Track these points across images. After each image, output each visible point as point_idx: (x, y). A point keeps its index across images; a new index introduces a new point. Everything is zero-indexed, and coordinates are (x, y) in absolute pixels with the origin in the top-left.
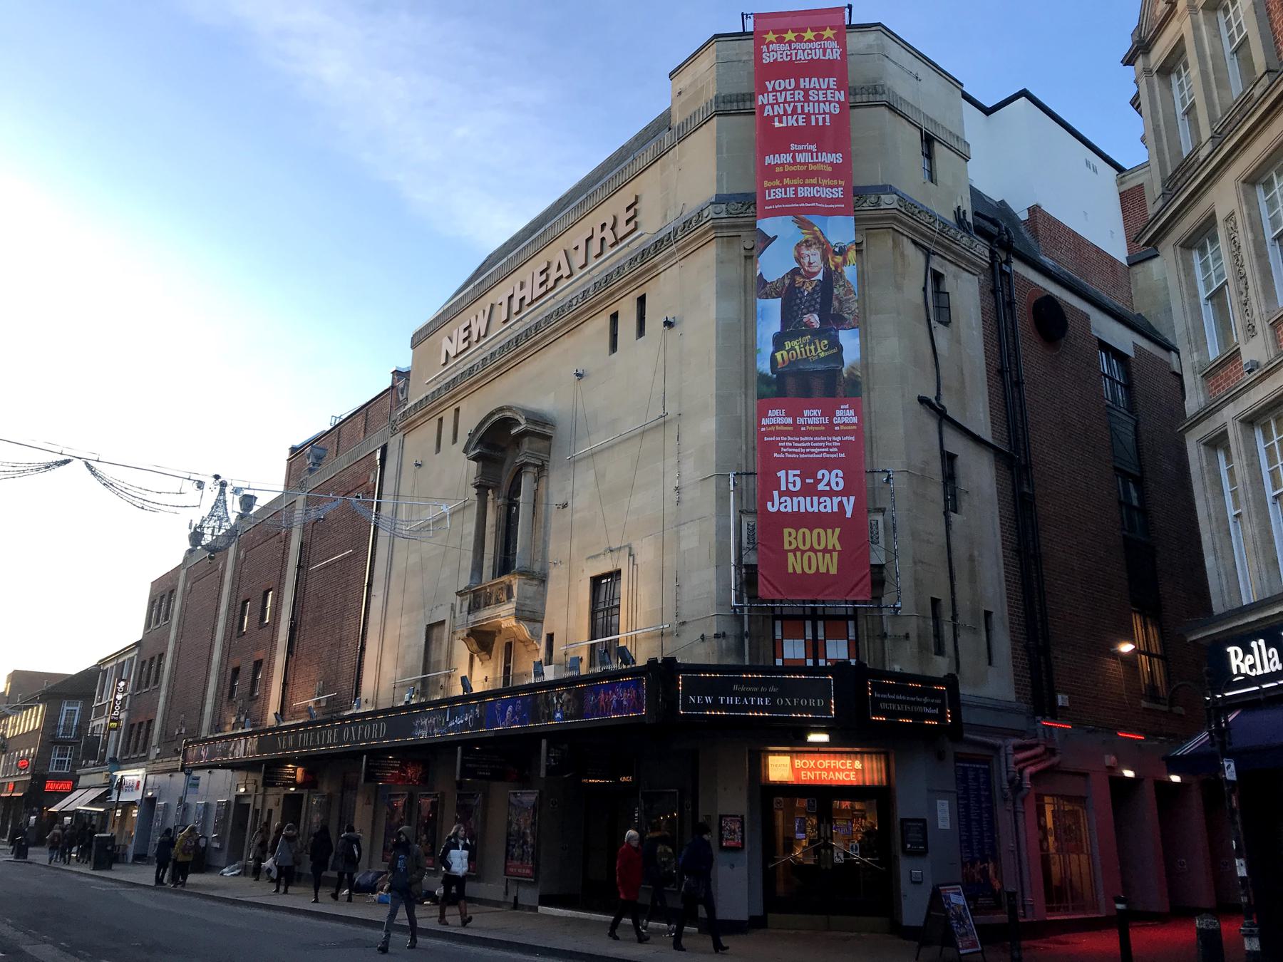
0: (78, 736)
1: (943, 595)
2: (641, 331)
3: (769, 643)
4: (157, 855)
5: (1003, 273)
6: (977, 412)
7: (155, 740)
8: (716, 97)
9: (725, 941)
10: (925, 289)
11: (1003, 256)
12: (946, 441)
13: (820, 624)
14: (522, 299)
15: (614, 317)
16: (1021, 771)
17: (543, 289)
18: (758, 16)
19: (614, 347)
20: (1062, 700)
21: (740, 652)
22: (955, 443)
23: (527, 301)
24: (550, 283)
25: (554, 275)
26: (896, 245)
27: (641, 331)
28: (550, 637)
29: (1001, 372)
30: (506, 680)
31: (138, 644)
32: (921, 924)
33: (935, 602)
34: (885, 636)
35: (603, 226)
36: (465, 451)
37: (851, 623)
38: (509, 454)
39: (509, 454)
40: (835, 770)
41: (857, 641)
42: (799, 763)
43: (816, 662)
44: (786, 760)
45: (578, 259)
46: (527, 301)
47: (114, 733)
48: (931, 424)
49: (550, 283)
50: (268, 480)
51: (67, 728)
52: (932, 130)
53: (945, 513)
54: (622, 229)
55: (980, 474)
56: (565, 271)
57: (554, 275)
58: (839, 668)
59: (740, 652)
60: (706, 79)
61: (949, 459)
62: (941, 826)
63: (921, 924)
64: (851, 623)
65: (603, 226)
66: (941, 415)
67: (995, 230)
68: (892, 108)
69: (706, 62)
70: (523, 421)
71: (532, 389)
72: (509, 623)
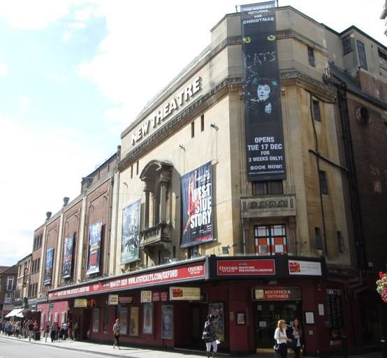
0: (13, 290)
1: (319, 225)
2: (203, 129)
3: (253, 247)
5: (343, 99)
6: (334, 154)
7: (39, 291)
10: (311, 108)
11: (343, 92)
12: (320, 166)
14: (160, 118)
17: (167, 114)
19: (193, 135)
22: (324, 166)
23: (162, 119)
24: (170, 112)
25: (171, 108)
26: (298, 92)
27: (203, 129)
29: (344, 138)
30: (184, 177)
31: (31, 255)
32: (312, 313)
33: (317, 229)
34: (297, 243)
35: (188, 89)
36: (140, 178)
40: (281, 294)
41: (286, 245)
43: (271, 254)
44: (262, 291)
45: (179, 102)
48: (314, 157)
50: (74, 191)
51: (10, 286)
52: (311, 45)
53: (321, 195)
54: (195, 90)
55: (336, 180)
56: (175, 107)
57: (171, 108)
58: (278, 255)
60: (223, 32)
61: (322, 174)
63: (312, 313)
64: (284, 238)
65: (188, 89)
66: (318, 156)
67: (339, 83)
68: (294, 38)
69: (224, 27)
70: (160, 166)
71: (160, 154)
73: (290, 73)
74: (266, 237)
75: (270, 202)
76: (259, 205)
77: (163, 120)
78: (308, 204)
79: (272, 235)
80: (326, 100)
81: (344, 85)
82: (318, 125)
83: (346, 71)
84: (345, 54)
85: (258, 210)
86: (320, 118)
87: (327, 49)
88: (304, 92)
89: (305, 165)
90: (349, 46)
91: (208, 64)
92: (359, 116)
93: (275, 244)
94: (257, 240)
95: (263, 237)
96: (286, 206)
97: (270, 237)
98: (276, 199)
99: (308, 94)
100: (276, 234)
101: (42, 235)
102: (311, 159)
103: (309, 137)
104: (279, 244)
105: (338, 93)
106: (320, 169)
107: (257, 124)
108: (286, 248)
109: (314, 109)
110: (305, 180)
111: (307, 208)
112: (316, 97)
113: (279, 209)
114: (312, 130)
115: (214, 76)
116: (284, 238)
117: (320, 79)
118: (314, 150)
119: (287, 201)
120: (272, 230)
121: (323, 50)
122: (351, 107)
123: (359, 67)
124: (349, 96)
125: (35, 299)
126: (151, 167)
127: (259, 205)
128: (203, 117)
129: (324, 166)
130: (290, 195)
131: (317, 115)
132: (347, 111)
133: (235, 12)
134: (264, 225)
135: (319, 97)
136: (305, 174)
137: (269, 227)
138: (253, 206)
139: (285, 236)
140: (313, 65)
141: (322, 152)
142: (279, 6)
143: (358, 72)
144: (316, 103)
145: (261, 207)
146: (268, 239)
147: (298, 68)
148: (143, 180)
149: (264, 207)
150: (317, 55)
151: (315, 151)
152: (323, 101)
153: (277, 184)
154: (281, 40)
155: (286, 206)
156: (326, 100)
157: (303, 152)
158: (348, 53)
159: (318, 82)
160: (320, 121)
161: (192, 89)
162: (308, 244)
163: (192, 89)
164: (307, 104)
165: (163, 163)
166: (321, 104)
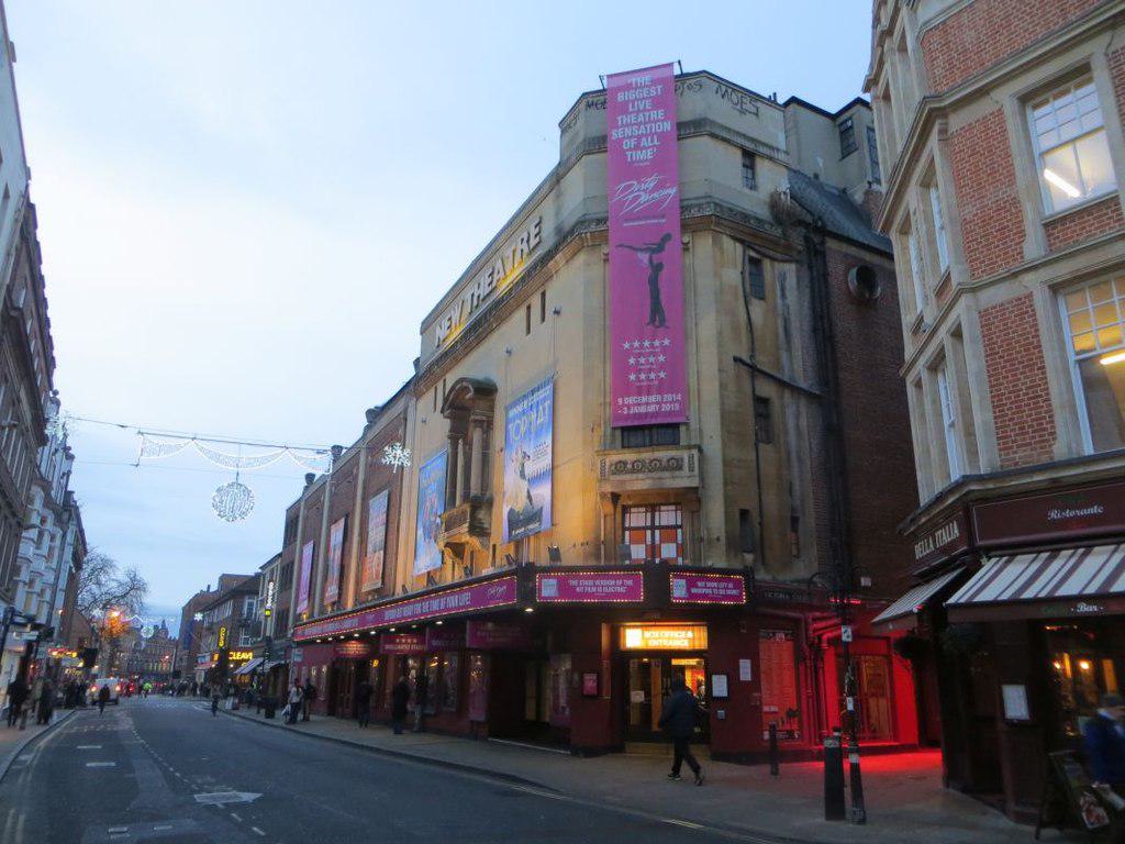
1: (751, 505)
4: (568, 703)
5: (817, 252)
6: (798, 364)
8: (584, 140)
9: (782, 766)
13: (657, 532)
15: (529, 308)
16: (820, 637)
18: (610, 76)
19: (543, 320)
20: (865, 581)
21: (598, 557)
23: (481, 297)
25: (496, 277)
26: (716, 242)
28: (494, 546)
29: (815, 330)
31: (280, 555)
33: (744, 514)
37: (679, 530)
38: (470, 410)
39: (470, 410)
42: (648, 634)
44: (638, 632)
46: (481, 297)
47: (269, 619)
48: (744, 371)
49: (494, 284)
52: (750, 146)
53: (756, 444)
54: (533, 242)
59: (598, 557)
62: (742, 678)
66: (754, 371)
67: (809, 219)
68: (713, 136)
71: (472, 368)
72: (466, 538)
73: (700, 206)
74: (645, 528)
75: (652, 461)
76: (629, 466)
77: (483, 300)
78: (726, 463)
79: (657, 524)
80: (779, 256)
81: (820, 224)
82: (757, 309)
83: (844, 191)
84: (841, 160)
85: (628, 477)
86: (763, 292)
87: (786, 153)
88: (727, 243)
89: (723, 386)
90: (851, 140)
91: (552, 195)
92: (853, 283)
93: (661, 542)
94: (627, 533)
95: (667, 527)
96: (680, 468)
97: (653, 528)
98: (664, 454)
99: (739, 247)
100: (664, 523)
101: (298, 517)
102: (738, 376)
103: (735, 329)
104: (637, 542)
105: (807, 239)
106: (757, 393)
107: (648, 305)
108: (681, 550)
109: (750, 274)
110: (722, 417)
111: (725, 473)
112: (753, 249)
113: (667, 474)
114: (743, 317)
115: (565, 213)
116: (679, 530)
117: (763, 212)
118: (745, 357)
119: (682, 460)
120: (657, 513)
121: (776, 155)
122: (836, 267)
123: (870, 183)
124: (831, 244)
125: (284, 641)
126: (460, 388)
127: (629, 466)
128: (543, 294)
129: (766, 389)
130: (689, 447)
131: (755, 286)
132: (825, 275)
133: (601, 88)
134: (641, 506)
135: (762, 250)
136: (722, 404)
137: (653, 508)
138: (620, 468)
139: (680, 527)
140: (753, 187)
141: (763, 362)
142: (684, 72)
143: (867, 193)
144: (755, 263)
145: (633, 471)
146: (649, 533)
147: (718, 195)
148: (445, 417)
149: (639, 471)
150: (763, 166)
151: (749, 361)
152: (773, 259)
153: (670, 431)
154: (688, 141)
155: (680, 468)
156: (779, 256)
157: (720, 362)
158: (849, 154)
159: (759, 220)
160: (762, 298)
161: (528, 241)
162: (723, 539)
163: (528, 241)
164: (736, 267)
165: (478, 382)
166: (767, 264)
